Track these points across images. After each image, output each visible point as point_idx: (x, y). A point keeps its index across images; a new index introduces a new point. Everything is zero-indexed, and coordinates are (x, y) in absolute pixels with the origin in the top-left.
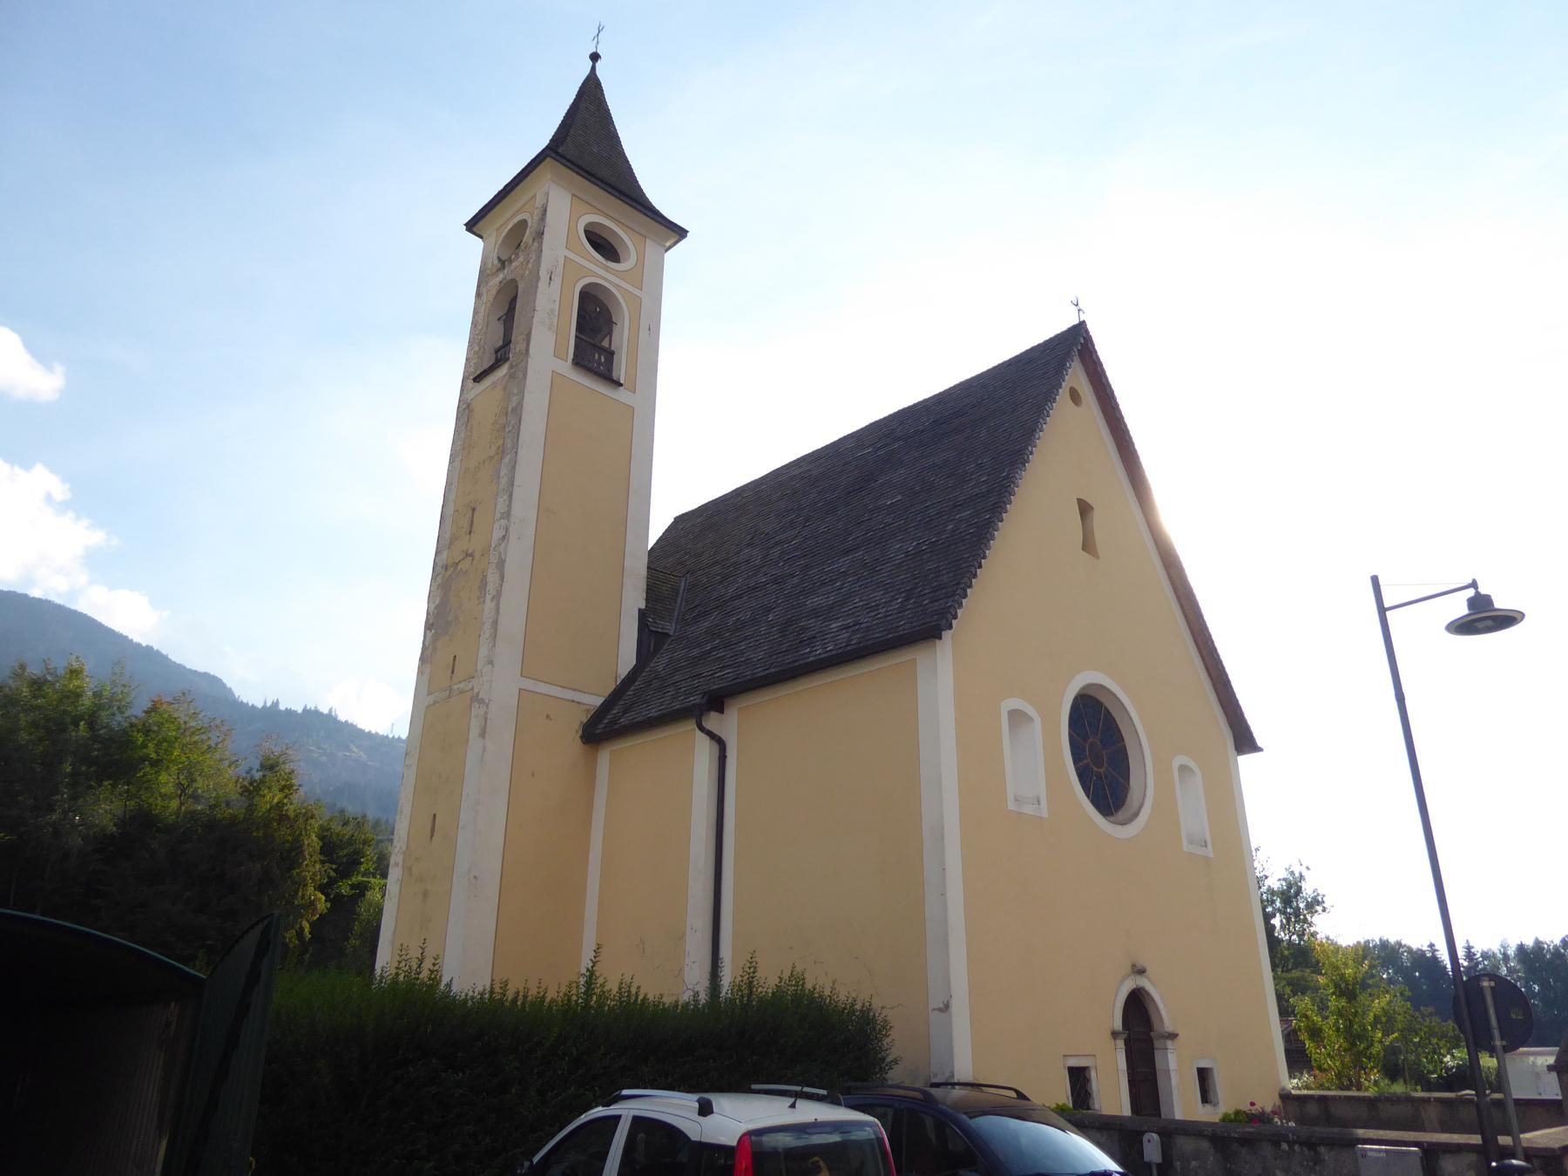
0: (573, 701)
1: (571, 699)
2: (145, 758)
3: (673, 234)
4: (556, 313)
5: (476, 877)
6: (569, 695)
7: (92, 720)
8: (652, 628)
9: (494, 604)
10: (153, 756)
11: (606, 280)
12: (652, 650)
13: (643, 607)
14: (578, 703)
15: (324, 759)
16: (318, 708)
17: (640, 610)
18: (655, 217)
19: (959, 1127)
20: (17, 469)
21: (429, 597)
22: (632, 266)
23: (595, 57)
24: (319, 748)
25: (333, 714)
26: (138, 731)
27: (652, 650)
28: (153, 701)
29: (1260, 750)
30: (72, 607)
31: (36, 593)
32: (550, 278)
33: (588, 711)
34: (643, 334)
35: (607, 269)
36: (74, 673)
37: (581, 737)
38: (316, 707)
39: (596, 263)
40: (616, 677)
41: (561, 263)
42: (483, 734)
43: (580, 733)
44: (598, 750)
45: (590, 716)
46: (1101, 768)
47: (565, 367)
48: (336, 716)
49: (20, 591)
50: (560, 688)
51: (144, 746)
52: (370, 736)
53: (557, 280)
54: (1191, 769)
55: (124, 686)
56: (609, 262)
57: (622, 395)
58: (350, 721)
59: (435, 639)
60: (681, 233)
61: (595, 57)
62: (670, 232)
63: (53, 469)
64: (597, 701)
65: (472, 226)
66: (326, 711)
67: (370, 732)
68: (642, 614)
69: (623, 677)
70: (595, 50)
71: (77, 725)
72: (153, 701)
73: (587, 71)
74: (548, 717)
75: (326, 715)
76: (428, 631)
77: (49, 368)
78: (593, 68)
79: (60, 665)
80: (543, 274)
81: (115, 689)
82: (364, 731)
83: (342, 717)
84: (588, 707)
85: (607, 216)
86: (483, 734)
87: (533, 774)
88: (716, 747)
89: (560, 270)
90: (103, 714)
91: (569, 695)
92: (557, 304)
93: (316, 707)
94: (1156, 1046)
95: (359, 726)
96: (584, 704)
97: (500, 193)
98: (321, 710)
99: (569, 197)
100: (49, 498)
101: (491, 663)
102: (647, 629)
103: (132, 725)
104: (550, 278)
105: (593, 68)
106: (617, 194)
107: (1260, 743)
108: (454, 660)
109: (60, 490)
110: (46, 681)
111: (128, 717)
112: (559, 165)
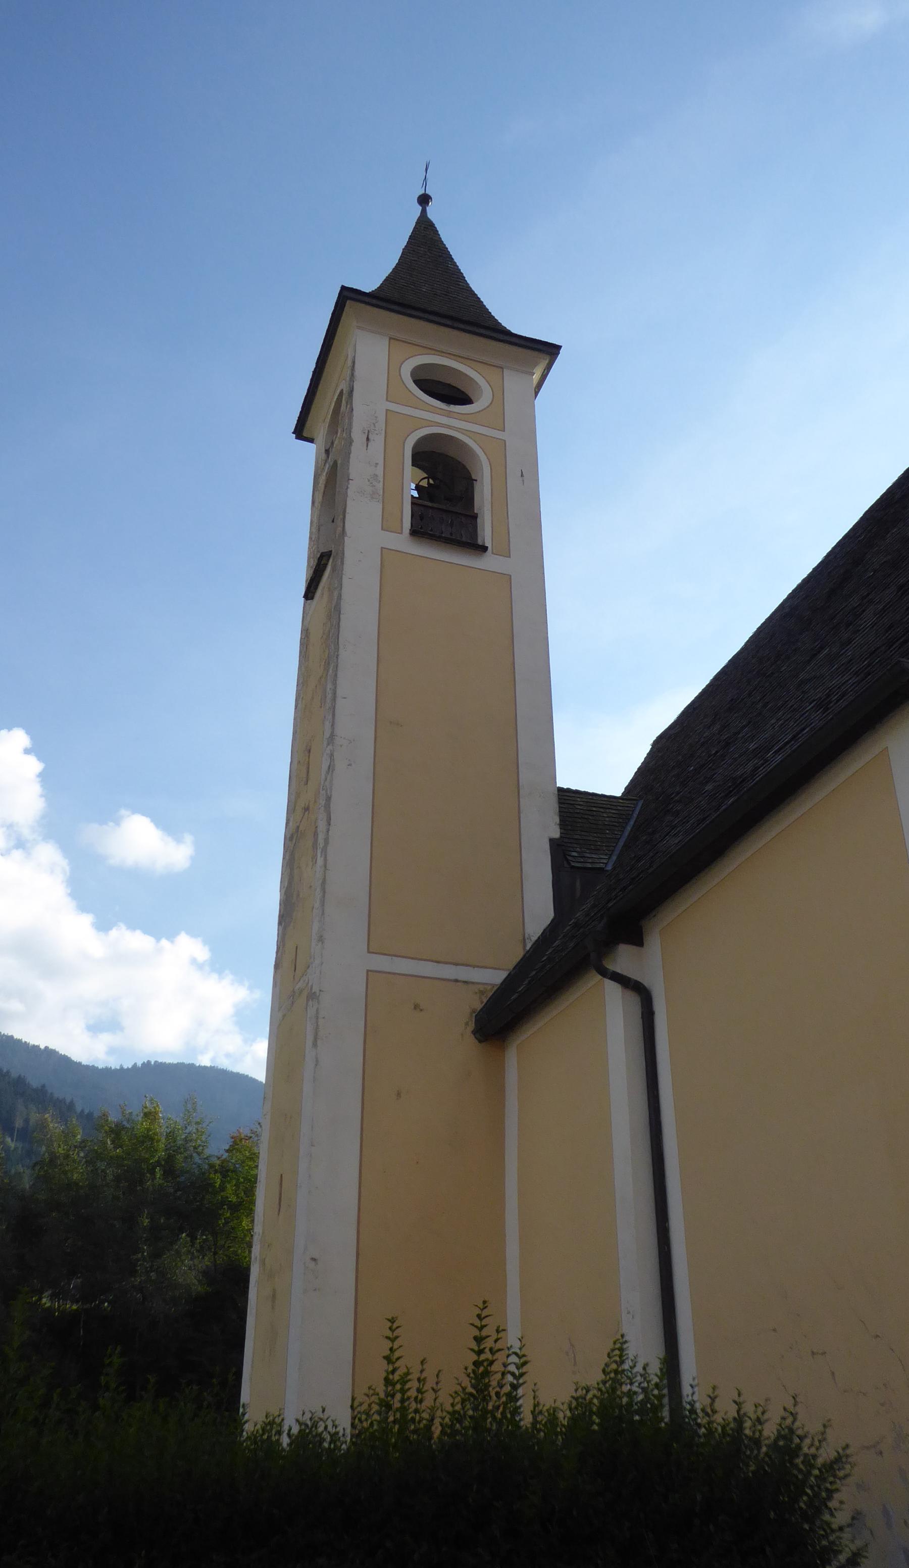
0: (456, 981)
1: (453, 977)
2: (224, 1201)
3: (541, 355)
5: (314, 1260)
6: (449, 972)
7: (169, 1169)
8: (573, 864)
9: (322, 858)
10: (233, 1199)
11: (449, 427)
12: (578, 893)
13: (556, 833)
14: (466, 982)
17: (552, 841)
18: (501, 337)
20: (164, 942)
21: (281, 882)
22: (487, 404)
23: (424, 200)
26: (216, 1172)
27: (578, 893)
28: (232, 1138)
30: (235, 1070)
31: (205, 1061)
32: (368, 439)
33: (482, 993)
34: (513, 482)
35: (449, 414)
36: (150, 1115)
37: (474, 1032)
39: (434, 410)
40: (524, 939)
41: (382, 418)
42: (315, 1044)
43: (472, 1026)
44: (504, 1051)
45: (485, 1001)
47: (402, 541)
49: (187, 1061)
50: (435, 964)
51: (223, 1188)
53: (378, 442)
55: (197, 1123)
57: (489, 562)
59: (285, 929)
60: (551, 350)
61: (424, 200)
62: (536, 353)
63: (192, 933)
64: (497, 977)
65: (300, 432)
68: (558, 849)
69: (534, 939)
71: (152, 1172)
72: (232, 1138)
74: (416, 1007)
76: (280, 927)
77: (179, 840)
78: (424, 212)
79: (135, 1110)
80: (357, 436)
81: (189, 1129)
84: (482, 988)
85: (442, 353)
86: (315, 1044)
87: (399, 1094)
88: (634, 1000)
89: (381, 425)
90: (179, 1157)
91: (449, 972)
96: (473, 983)
97: (314, 372)
99: (386, 341)
100: (194, 961)
101: (321, 939)
102: (566, 865)
103: (212, 1166)
104: (368, 439)
105: (424, 212)
106: (449, 322)
108: (297, 949)
109: (202, 953)
110: (124, 1128)
111: (207, 1158)
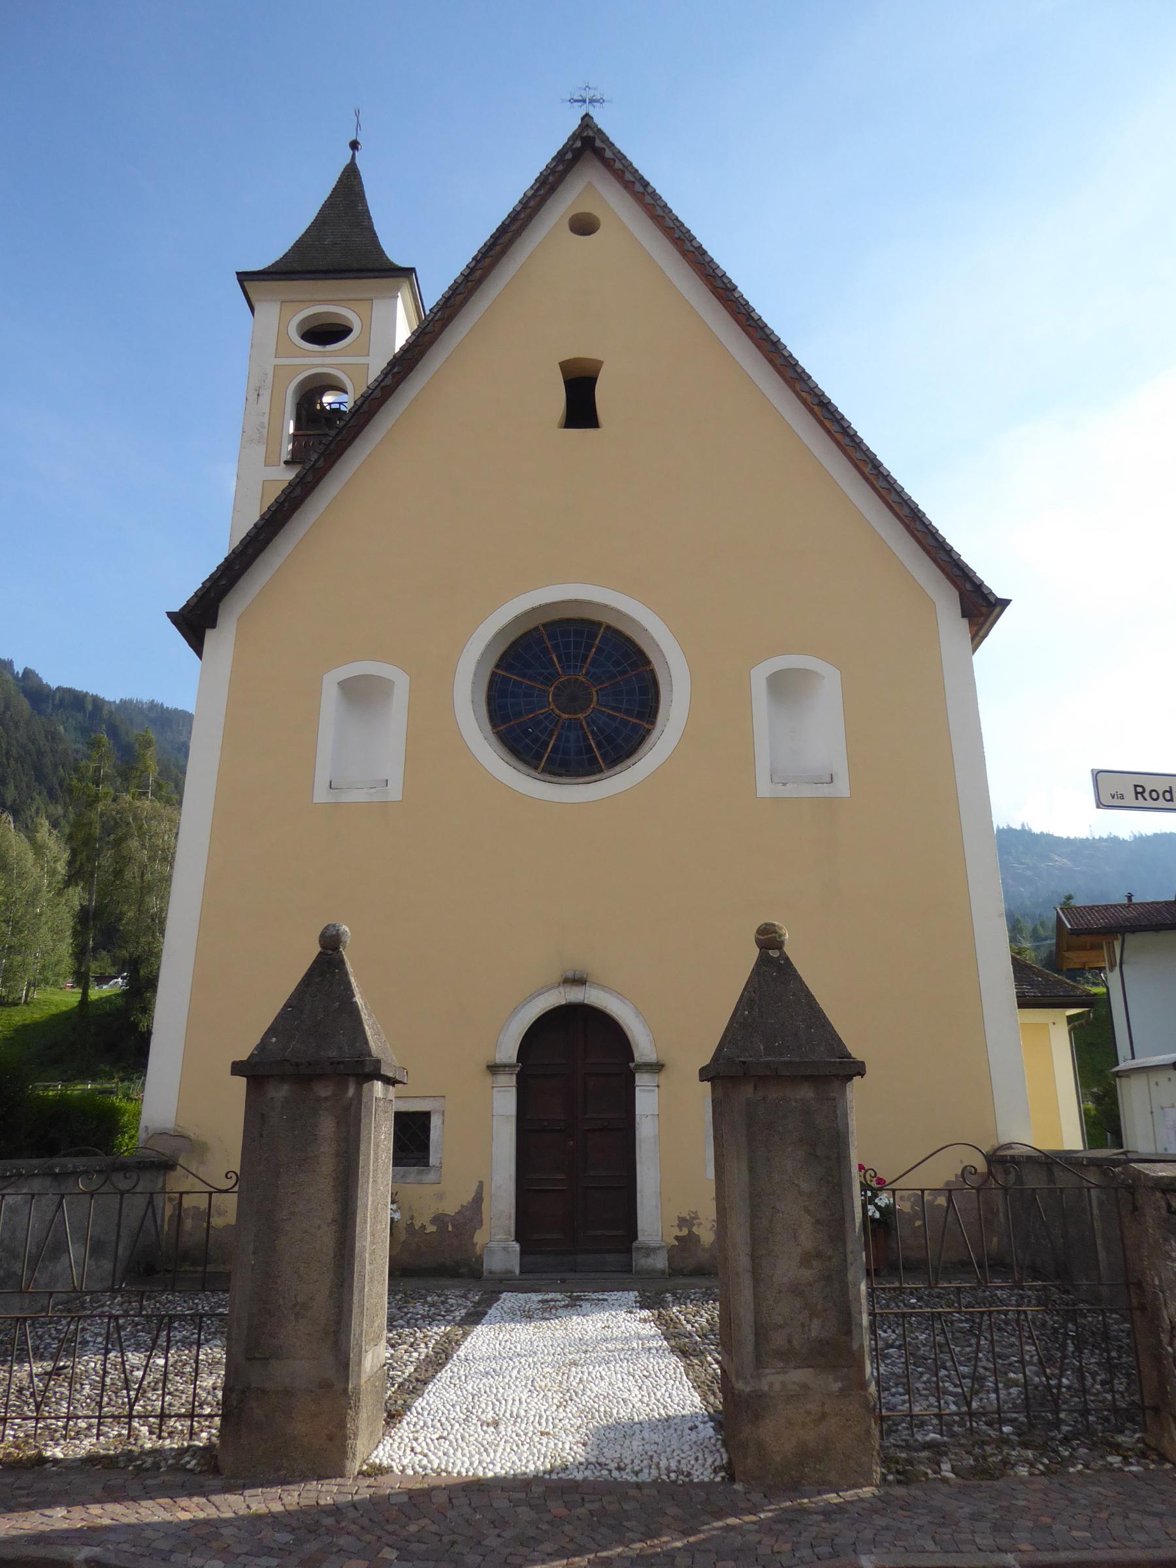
4: (267, 426)
15: (1028, 873)
16: (1011, 826)
19: (1008, 1216)
23: (354, 145)
24: (1022, 863)
25: (1027, 828)
29: (1005, 603)
38: (1008, 825)
41: (270, 372)
46: (583, 710)
48: (1030, 830)
52: (1068, 841)
54: (816, 672)
56: (327, 346)
58: (1045, 831)
61: (354, 145)
66: (1019, 827)
67: (1068, 839)
70: (354, 138)
73: (348, 161)
75: (1020, 831)
78: (353, 156)
82: (1062, 838)
83: (1037, 830)
92: (267, 416)
93: (1008, 825)
94: (637, 1083)
95: (1056, 835)
98: (1014, 827)
105: (353, 156)
107: (1000, 594)
112: (256, 283)
